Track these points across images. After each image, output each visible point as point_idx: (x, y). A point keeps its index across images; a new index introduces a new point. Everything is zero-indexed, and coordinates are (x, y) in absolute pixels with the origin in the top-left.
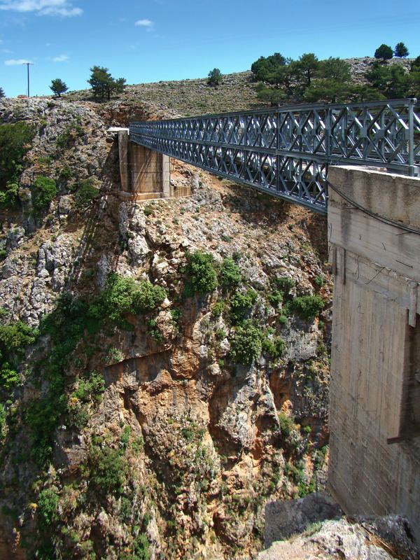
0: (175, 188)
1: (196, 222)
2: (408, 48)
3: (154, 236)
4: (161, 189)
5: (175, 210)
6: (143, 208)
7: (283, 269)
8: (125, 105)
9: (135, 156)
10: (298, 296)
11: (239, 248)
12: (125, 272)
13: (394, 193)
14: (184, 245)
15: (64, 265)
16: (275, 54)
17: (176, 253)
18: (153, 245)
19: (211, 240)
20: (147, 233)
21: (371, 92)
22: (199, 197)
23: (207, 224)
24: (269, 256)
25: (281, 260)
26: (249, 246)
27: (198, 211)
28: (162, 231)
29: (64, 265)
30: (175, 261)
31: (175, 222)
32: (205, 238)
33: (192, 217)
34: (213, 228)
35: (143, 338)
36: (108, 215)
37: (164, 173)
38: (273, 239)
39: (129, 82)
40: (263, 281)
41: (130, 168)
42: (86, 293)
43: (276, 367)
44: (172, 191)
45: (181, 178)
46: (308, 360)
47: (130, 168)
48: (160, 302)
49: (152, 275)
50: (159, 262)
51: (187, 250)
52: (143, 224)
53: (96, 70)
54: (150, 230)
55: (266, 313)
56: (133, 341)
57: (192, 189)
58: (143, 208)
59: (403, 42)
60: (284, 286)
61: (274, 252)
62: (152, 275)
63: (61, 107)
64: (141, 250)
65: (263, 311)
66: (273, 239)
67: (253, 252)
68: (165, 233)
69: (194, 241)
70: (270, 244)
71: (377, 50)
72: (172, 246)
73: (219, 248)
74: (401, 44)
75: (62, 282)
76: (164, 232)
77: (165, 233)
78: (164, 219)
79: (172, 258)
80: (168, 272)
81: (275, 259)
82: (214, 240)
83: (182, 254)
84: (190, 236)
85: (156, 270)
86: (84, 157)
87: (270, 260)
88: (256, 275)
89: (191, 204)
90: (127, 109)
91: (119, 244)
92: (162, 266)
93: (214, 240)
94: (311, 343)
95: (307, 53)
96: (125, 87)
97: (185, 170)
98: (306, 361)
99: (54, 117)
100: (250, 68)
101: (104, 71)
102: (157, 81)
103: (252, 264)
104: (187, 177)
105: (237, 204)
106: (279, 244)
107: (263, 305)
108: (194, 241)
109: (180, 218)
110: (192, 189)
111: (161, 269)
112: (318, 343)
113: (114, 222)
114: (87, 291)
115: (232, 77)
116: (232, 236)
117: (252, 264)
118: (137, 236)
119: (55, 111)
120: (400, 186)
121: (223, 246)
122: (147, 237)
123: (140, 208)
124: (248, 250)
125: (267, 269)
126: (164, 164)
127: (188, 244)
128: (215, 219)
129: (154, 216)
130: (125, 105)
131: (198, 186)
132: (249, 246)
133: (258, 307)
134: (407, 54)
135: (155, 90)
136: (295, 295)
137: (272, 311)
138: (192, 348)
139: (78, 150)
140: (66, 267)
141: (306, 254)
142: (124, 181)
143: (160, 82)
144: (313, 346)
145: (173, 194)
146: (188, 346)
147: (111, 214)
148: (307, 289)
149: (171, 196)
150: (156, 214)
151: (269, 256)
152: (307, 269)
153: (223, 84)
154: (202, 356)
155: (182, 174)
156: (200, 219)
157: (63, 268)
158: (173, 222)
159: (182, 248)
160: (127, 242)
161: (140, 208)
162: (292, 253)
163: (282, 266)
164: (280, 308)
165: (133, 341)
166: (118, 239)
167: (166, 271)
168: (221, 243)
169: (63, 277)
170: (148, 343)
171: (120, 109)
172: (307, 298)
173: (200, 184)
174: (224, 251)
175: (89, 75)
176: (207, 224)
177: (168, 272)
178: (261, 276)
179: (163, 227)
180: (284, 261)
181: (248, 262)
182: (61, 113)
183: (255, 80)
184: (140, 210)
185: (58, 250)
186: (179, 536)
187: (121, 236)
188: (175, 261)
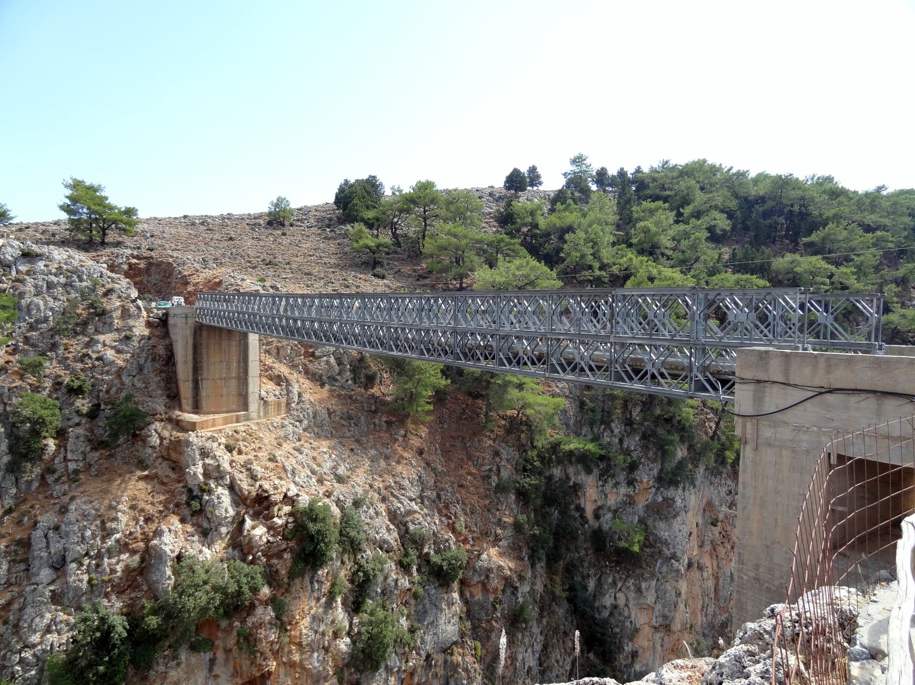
0: (265, 402)
1: (300, 457)
2: (776, 168)
3: (245, 484)
4: (245, 406)
5: (268, 438)
6: (223, 440)
7: (417, 516)
8: (137, 257)
9: (204, 350)
10: (436, 552)
11: (360, 491)
12: (201, 551)
14: (290, 494)
15: (87, 554)
16: (370, 176)
17: (279, 510)
18: (238, 498)
19: (322, 484)
20: (233, 479)
21: (510, 244)
22: (298, 416)
23: (314, 459)
24: (398, 498)
25: (413, 503)
26: (371, 486)
27: (299, 440)
28: (256, 476)
30: (279, 521)
31: (272, 459)
32: (314, 480)
33: (294, 449)
34: (323, 464)
35: (227, 660)
36: (162, 457)
37: (250, 380)
38: (401, 473)
39: (143, 214)
40: (392, 537)
41: (197, 369)
42: (131, 599)
43: (411, 667)
45: (271, 386)
47: (197, 369)
48: (255, 590)
49: (242, 550)
50: (253, 528)
51: (293, 501)
53: (76, 185)
54: (238, 476)
55: (396, 584)
57: (288, 404)
58: (223, 440)
59: (537, 166)
61: (403, 492)
62: (242, 550)
63: (49, 259)
65: (393, 584)
66: (401, 473)
67: (376, 495)
68: (261, 478)
69: (302, 487)
70: (398, 479)
71: (425, 187)
72: (273, 498)
73: (335, 493)
74: (602, 169)
75: (84, 586)
77: (261, 478)
79: (273, 517)
80: (268, 541)
81: (406, 502)
82: (326, 483)
83: (287, 509)
86: (110, 354)
87: (399, 505)
89: (290, 428)
90: (142, 265)
91: (188, 504)
92: (259, 532)
93: (326, 483)
94: (452, 621)
95: (423, 180)
96: (136, 223)
98: (446, 650)
99: (41, 277)
100: (331, 199)
101: (93, 189)
102: (180, 214)
103: (377, 513)
106: (409, 479)
107: (393, 574)
108: (302, 487)
109: (278, 453)
110: (288, 404)
112: (461, 618)
113: (173, 469)
114: (133, 595)
115: (304, 212)
117: (377, 513)
118: (216, 487)
119: (41, 265)
121: (339, 490)
122: (232, 488)
123: (219, 441)
124: (371, 494)
126: (250, 363)
127: (296, 492)
128: (325, 450)
129: (240, 452)
130: (137, 257)
131: (296, 399)
132: (371, 486)
134: (540, 183)
135: (183, 231)
136: (432, 552)
137: (405, 582)
138: (301, 660)
140: (90, 557)
141: (442, 489)
142: (186, 389)
143: (185, 217)
144: (454, 625)
145: (262, 414)
148: (447, 541)
149: (259, 417)
150: (243, 448)
151: (398, 498)
152: (445, 512)
153: (292, 225)
154: (315, 671)
155: (271, 380)
157: (86, 561)
158: (270, 460)
159: (288, 499)
162: (425, 490)
163: (415, 512)
164: (415, 574)
165: (211, 670)
167: (265, 540)
168: (336, 485)
169: (86, 577)
170: (235, 667)
171: (130, 265)
173: (300, 395)
174: (342, 498)
175: (62, 195)
176: (314, 459)
177: (268, 541)
178: (388, 530)
179: (257, 468)
180: (416, 504)
181: (372, 511)
182: (54, 271)
183: (342, 221)
184: (220, 444)
187: (190, 491)
188: (279, 521)
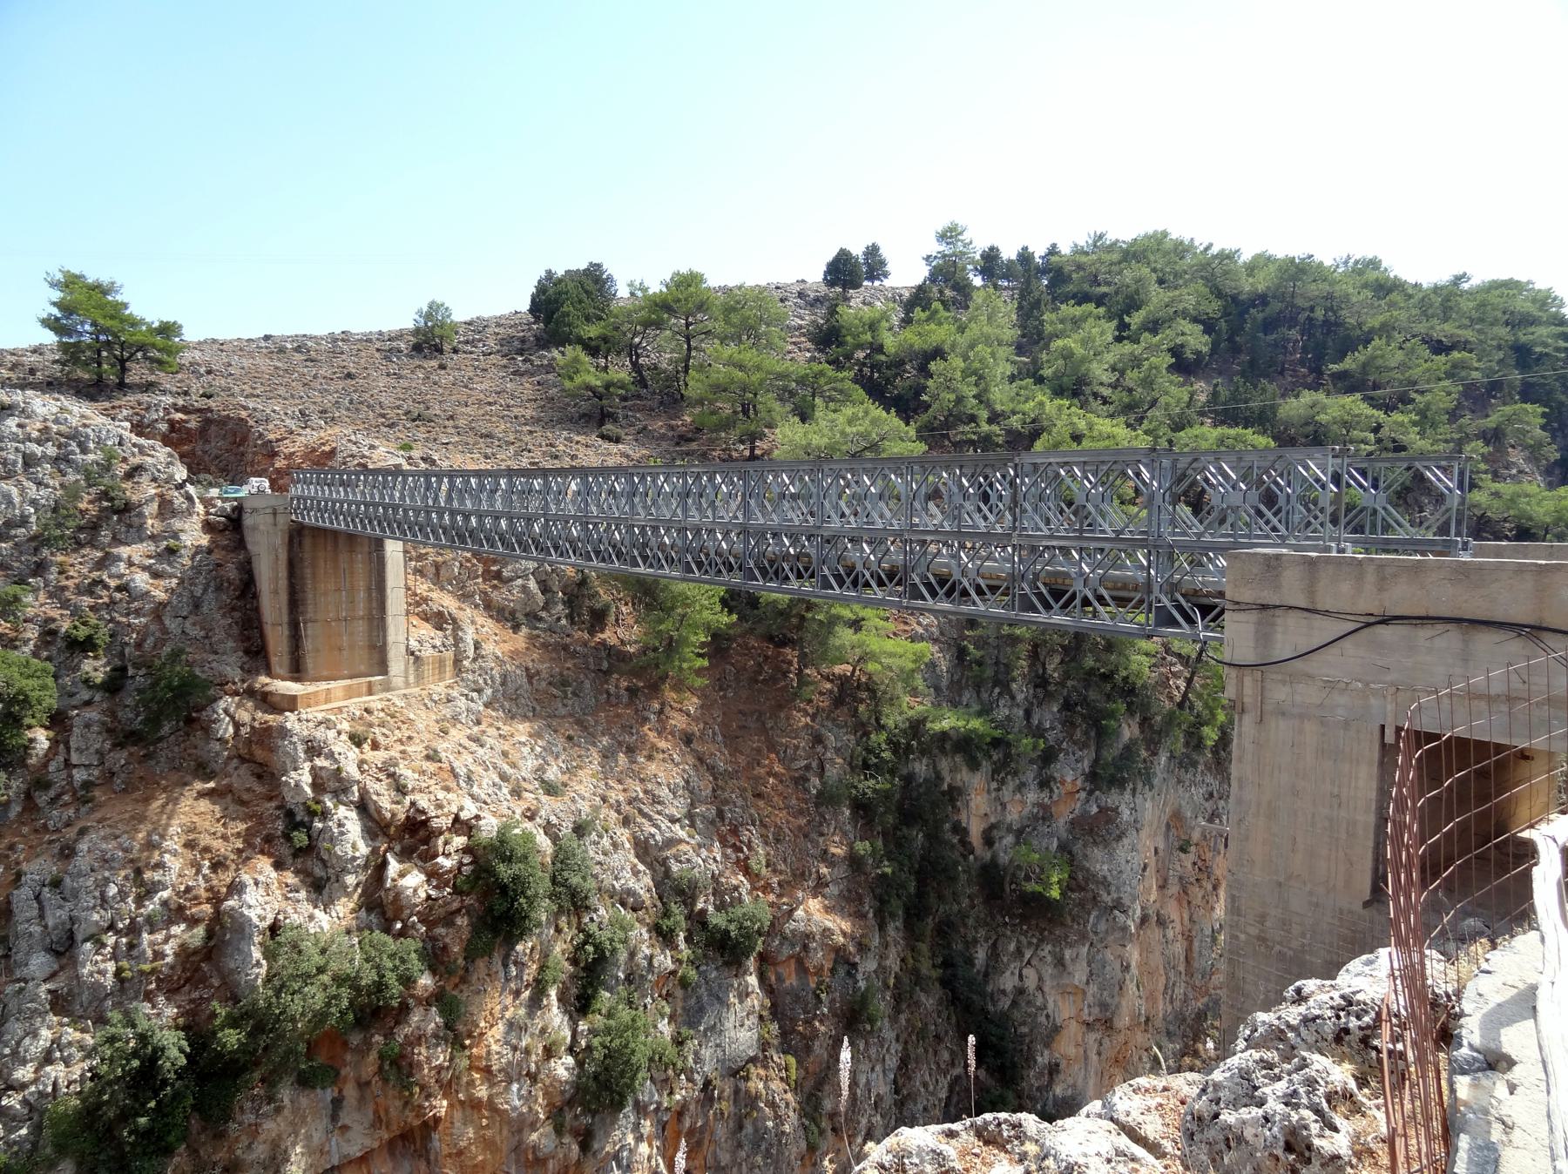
0: (417, 658)
1: (481, 751)
3: (385, 801)
6: (345, 726)
7: (683, 847)
8: (184, 410)
10: (718, 909)
11: (585, 807)
12: (311, 917)
13: (1360, 578)
14: (464, 815)
17: (446, 843)
18: (374, 825)
19: (520, 797)
20: (364, 793)
22: (475, 682)
23: (505, 754)
24: (650, 819)
25: (677, 826)
26: (604, 799)
27: (478, 723)
29: (111, 927)
31: (432, 756)
32: (505, 791)
33: (470, 738)
34: (521, 763)
37: (390, 620)
40: (642, 885)
41: (295, 602)
42: (191, 1001)
43: (678, 1102)
44: (411, 670)
46: (742, 1068)
47: (295, 602)
49: (383, 913)
50: (402, 875)
52: (351, 770)
53: (70, 282)
54: (372, 786)
56: (334, 1118)
57: (457, 662)
58: (345, 726)
59: (880, 243)
60: (685, 892)
61: (659, 808)
62: (383, 913)
64: (354, 847)
65: (645, 963)
67: (613, 815)
68: (413, 790)
69: (485, 803)
70: (650, 787)
72: (435, 823)
73: (543, 813)
76: (410, 787)
78: (403, 752)
79: (437, 856)
83: (460, 841)
84: (475, 789)
85: (398, 895)
87: (653, 830)
88: (627, 874)
90: (193, 423)
92: (412, 882)
93: (526, 795)
95: (684, 270)
97: (435, 608)
98: (737, 1072)
100: (524, 305)
101: (100, 290)
102: (257, 333)
103: (615, 845)
104: (441, 629)
105: (565, 692)
107: (644, 947)
108: (485, 803)
109: (441, 746)
111: (409, 892)
113: (259, 777)
114: (195, 995)
115: (477, 327)
116: (565, 778)
117: (615, 845)
118: (336, 807)
120: (1371, 569)
121: (550, 807)
123: (339, 727)
125: (643, 849)
126: (389, 591)
127: (475, 812)
128: (523, 739)
129: (375, 746)
130: (184, 410)
131: (471, 653)
132: (604, 799)
133: (632, 955)
134: (886, 275)
135: (264, 363)
136: (711, 908)
137: (665, 961)
138: (490, 1097)
139: (119, 559)
140: (118, 932)
144: (750, 1029)
145: (412, 679)
146: (479, 1094)
147: (251, 754)
149: (407, 685)
150: (381, 739)
151: (650, 819)
152: (732, 840)
153: (455, 351)
154: (514, 1115)
155: (427, 620)
156: (490, 741)
157: (110, 939)
158: (428, 758)
159: (461, 825)
160: (309, 828)
161: (339, 727)
163: (681, 841)
166: (280, 825)
168: (544, 799)
169: (111, 967)
170: (376, 1112)
171: (172, 423)
172: (739, 911)
173: (477, 646)
174: (554, 820)
175: (45, 301)
176: (505, 754)
177: (429, 897)
178: (636, 873)
181: (606, 842)
182: (35, 434)
183: (543, 343)
184: (339, 733)
185: (90, 882)
186: (1492, 1111)
187: (290, 814)
188: (446, 863)
